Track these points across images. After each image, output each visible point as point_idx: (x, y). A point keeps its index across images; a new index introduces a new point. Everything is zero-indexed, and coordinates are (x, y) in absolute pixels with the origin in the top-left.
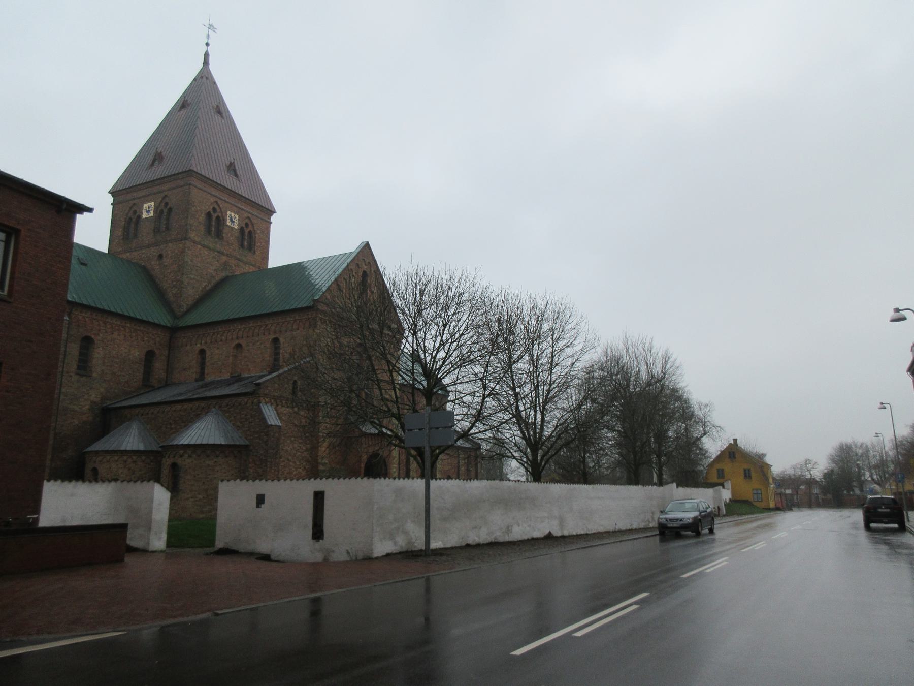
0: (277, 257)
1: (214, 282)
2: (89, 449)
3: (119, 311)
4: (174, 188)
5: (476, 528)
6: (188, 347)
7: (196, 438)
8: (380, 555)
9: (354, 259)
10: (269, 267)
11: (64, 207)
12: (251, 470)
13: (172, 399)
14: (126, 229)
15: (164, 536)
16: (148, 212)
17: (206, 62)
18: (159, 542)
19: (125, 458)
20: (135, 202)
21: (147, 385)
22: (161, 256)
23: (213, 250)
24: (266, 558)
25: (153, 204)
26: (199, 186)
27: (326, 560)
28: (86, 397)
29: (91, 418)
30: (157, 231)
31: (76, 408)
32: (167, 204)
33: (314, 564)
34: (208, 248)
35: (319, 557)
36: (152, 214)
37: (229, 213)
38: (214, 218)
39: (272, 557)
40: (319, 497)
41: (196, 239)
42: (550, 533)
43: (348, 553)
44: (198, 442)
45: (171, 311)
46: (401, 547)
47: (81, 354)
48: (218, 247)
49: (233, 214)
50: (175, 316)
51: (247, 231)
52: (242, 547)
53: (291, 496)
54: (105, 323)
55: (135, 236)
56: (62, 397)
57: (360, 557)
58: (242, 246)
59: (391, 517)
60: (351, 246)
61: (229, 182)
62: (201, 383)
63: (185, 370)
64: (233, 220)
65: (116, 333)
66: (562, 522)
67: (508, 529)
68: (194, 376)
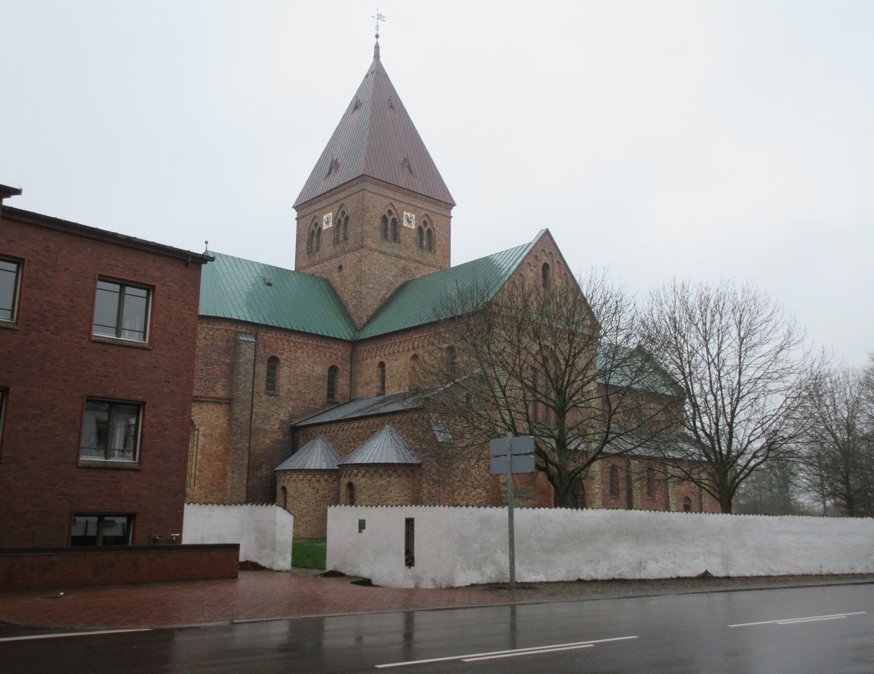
0: (460, 255)
1: (393, 289)
2: (277, 469)
3: (301, 329)
4: (349, 196)
5: (591, 561)
6: (369, 360)
7: (368, 457)
8: (463, 585)
9: (531, 250)
10: (452, 266)
11: (190, 260)
12: (425, 491)
13: (350, 417)
14: (310, 242)
15: (289, 557)
16: (327, 223)
17: (377, 56)
18: (285, 562)
19: (309, 477)
20: (315, 214)
21: (332, 400)
22: (341, 267)
23: (390, 255)
24: (366, 582)
25: (331, 214)
26: (374, 190)
27: (417, 587)
28: (275, 416)
29: (281, 437)
30: (336, 242)
31: (267, 428)
32: (343, 213)
33: (408, 590)
34: (385, 253)
35: (411, 584)
36: (331, 225)
37: (405, 213)
38: (390, 221)
39: (373, 582)
40: (410, 523)
41: (373, 246)
42: (707, 572)
43: (434, 580)
44: (371, 461)
45: (352, 324)
46: (490, 578)
47: (268, 374)
48: (396, 251)
49: (409, 214)
50: (356, 330)
51: (425, 230)
52: (348, 571)
53: (387, 520)
54: (288, 341)
55: (318, 248)
56: (254, 417)
57: (443, 587)
58: (421, 246)
59: (476, 546)
60: (529, 237)
61: (402, 180)
62: (381, 398)
63: (367, 384)
64: (410, 220)
65: (299, 351)
66: (726, 559)
67: (641, 565)
68: (376, 390)
